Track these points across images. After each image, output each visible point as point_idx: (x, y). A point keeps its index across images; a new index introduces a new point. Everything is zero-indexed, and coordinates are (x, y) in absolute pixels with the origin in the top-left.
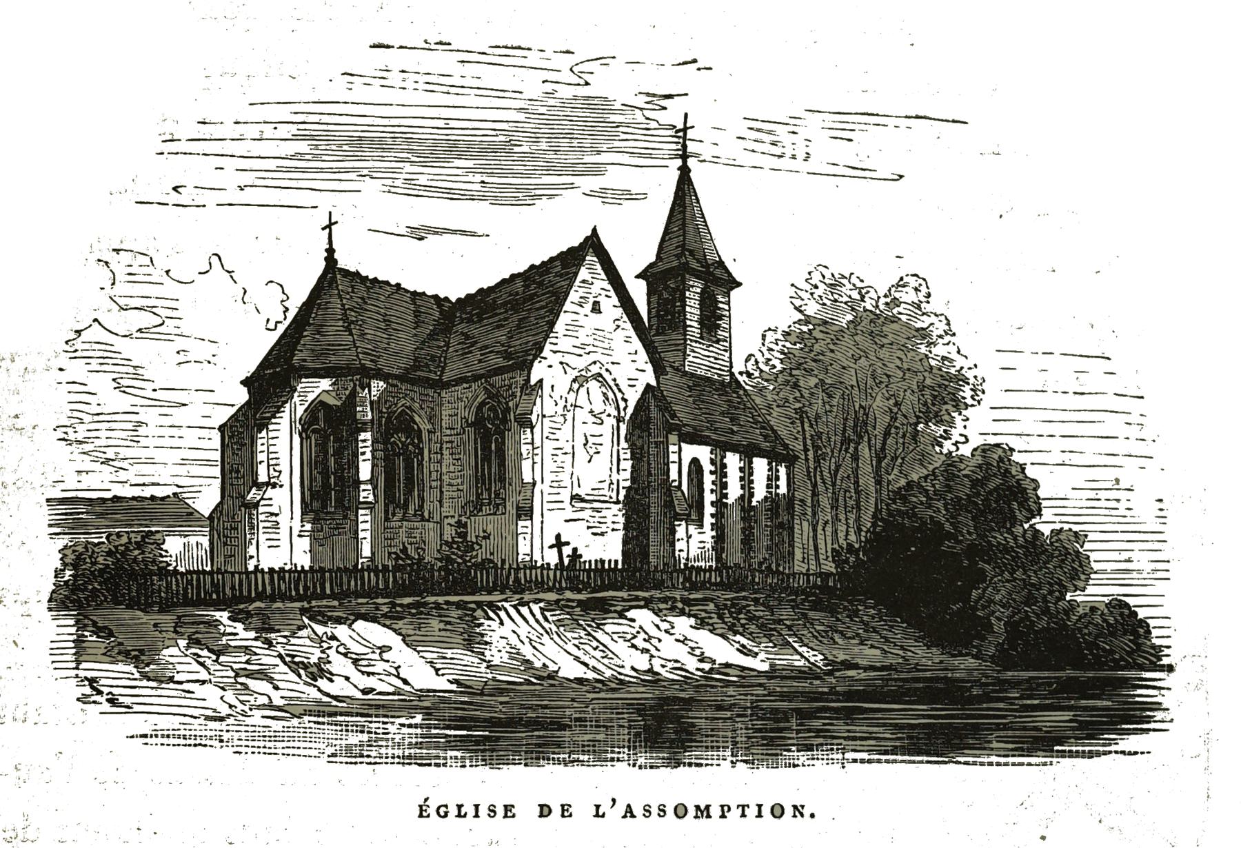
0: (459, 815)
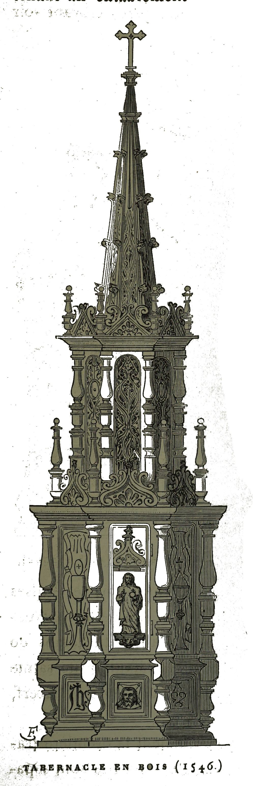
0: (93, 769)
